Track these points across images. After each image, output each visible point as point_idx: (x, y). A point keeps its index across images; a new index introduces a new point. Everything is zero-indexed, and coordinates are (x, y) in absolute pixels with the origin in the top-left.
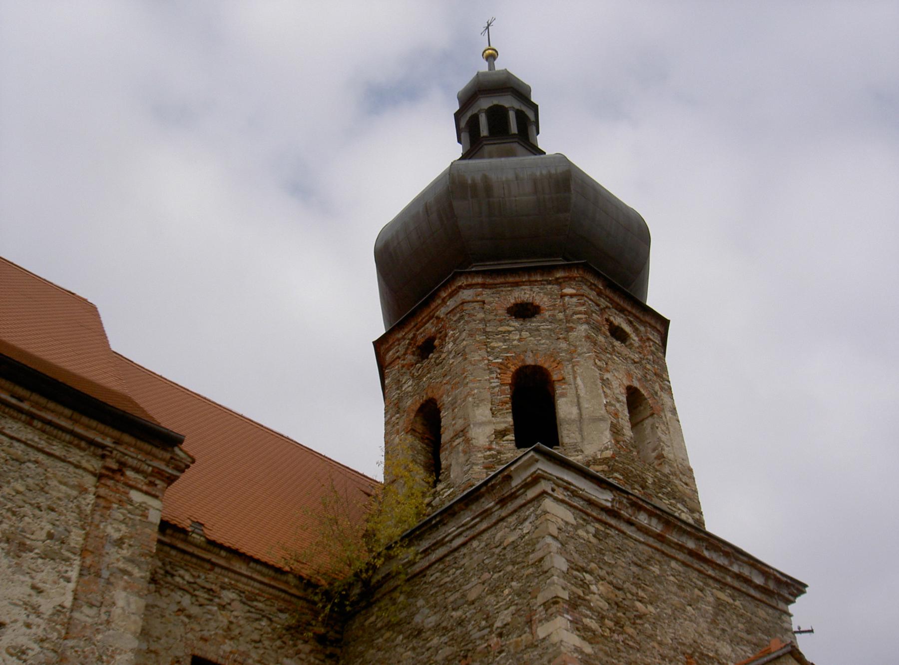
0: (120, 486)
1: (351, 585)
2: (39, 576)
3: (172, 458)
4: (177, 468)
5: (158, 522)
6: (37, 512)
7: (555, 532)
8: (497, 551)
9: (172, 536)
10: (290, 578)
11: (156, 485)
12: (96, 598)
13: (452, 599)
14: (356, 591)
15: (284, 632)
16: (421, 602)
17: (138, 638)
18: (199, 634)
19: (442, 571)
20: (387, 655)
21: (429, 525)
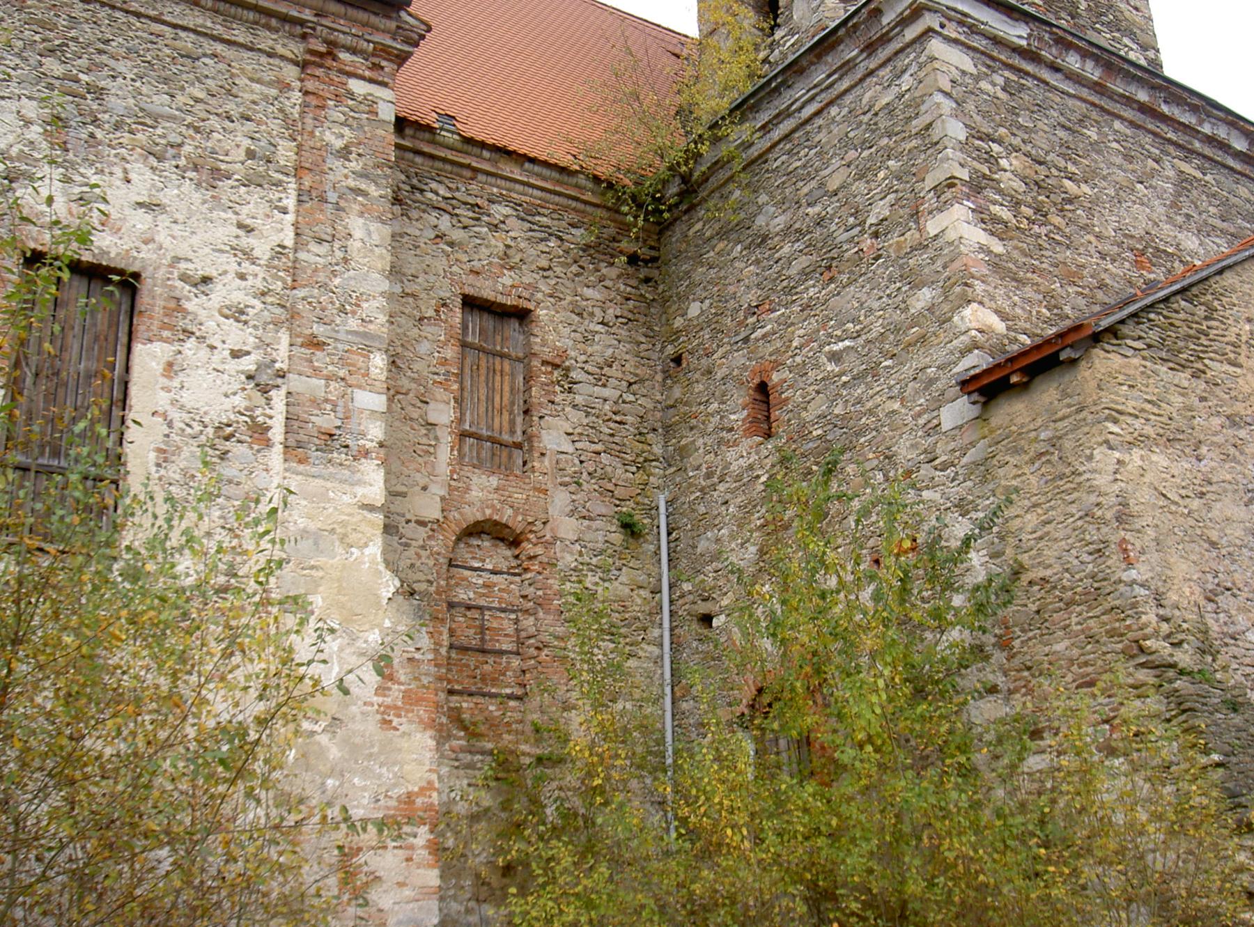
0: (333, 75)
1: (665, 182)
2: (245, 210)
3: (398, 27)
4: (406, 41)
5: (393, 119)
6: (227, 124)
7: (947, 86)
8: (865, 118)
9: (413, 137)
10: (581, 180)
11: (382, 68)
12: (325, 230)
13: (805, 190)
14: (673, 189)
15: (581, 253)
16: (763, 198)
17: (387, 278)
18: (467, 267)
19: (789, 152)
20: (722, 274)
21: (768, 90)
